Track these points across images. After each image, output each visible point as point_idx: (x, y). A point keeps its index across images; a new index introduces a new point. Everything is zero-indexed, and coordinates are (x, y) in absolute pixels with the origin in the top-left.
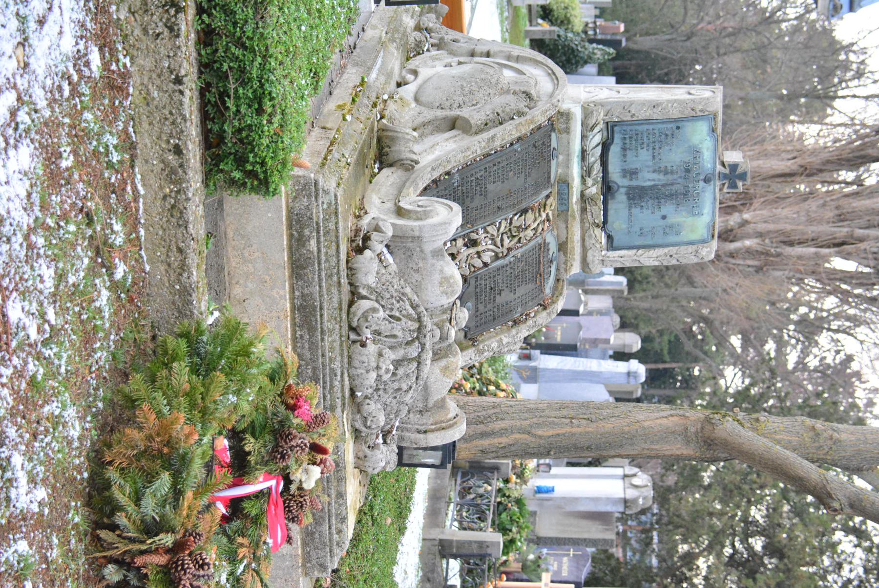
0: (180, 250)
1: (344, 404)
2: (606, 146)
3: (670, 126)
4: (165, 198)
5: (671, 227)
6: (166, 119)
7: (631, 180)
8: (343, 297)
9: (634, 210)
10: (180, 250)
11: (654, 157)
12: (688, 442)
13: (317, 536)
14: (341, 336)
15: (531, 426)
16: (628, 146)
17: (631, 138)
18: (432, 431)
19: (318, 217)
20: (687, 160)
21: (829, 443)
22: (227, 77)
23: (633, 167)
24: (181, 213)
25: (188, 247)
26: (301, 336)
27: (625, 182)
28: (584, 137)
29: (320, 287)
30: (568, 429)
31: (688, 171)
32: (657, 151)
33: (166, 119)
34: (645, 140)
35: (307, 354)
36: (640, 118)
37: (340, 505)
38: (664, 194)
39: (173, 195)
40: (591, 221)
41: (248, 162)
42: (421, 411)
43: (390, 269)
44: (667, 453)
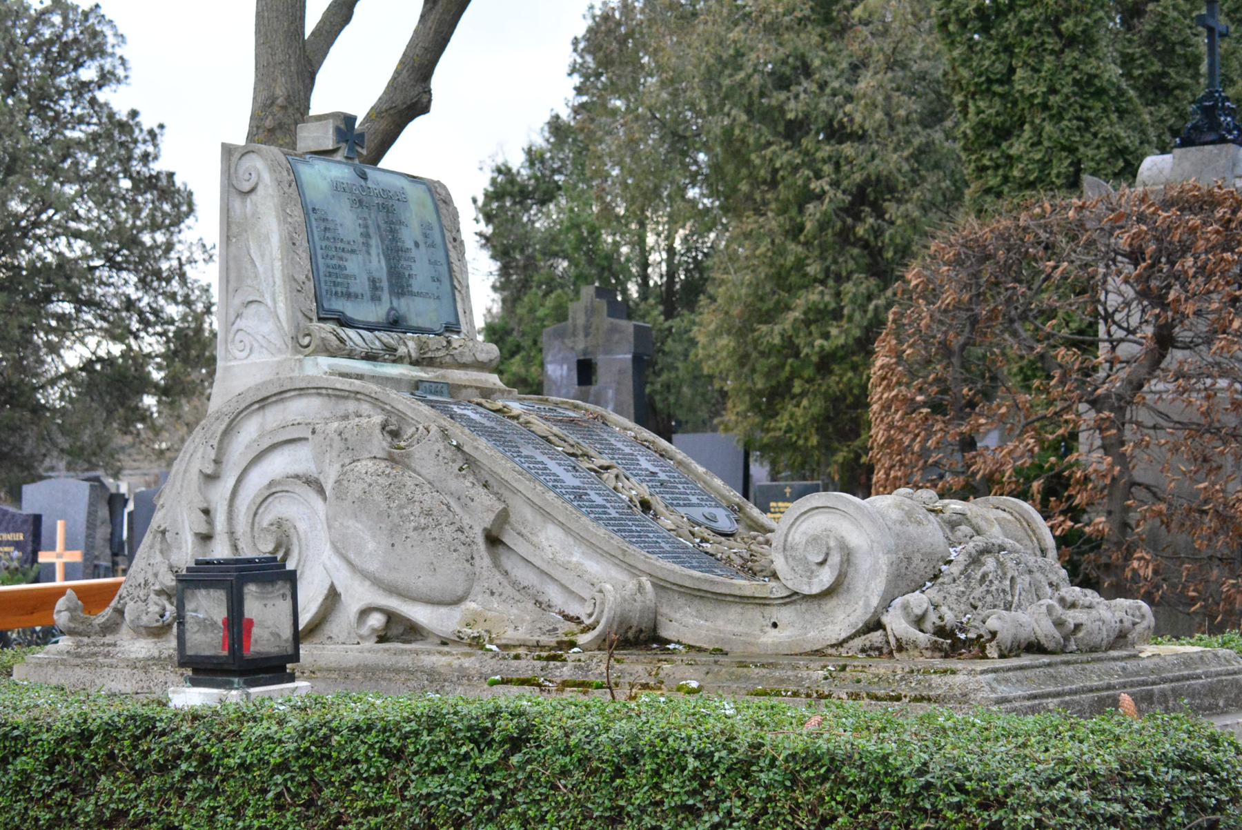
5: (426, 236)
8: (979, 668)
9: (415, 289)
17: (335, 284)
21: (290, 110)
23: (367, 283)
29: (1025, 698)
32: (348, 247)
36: (309, 267)
43: (937, 598)
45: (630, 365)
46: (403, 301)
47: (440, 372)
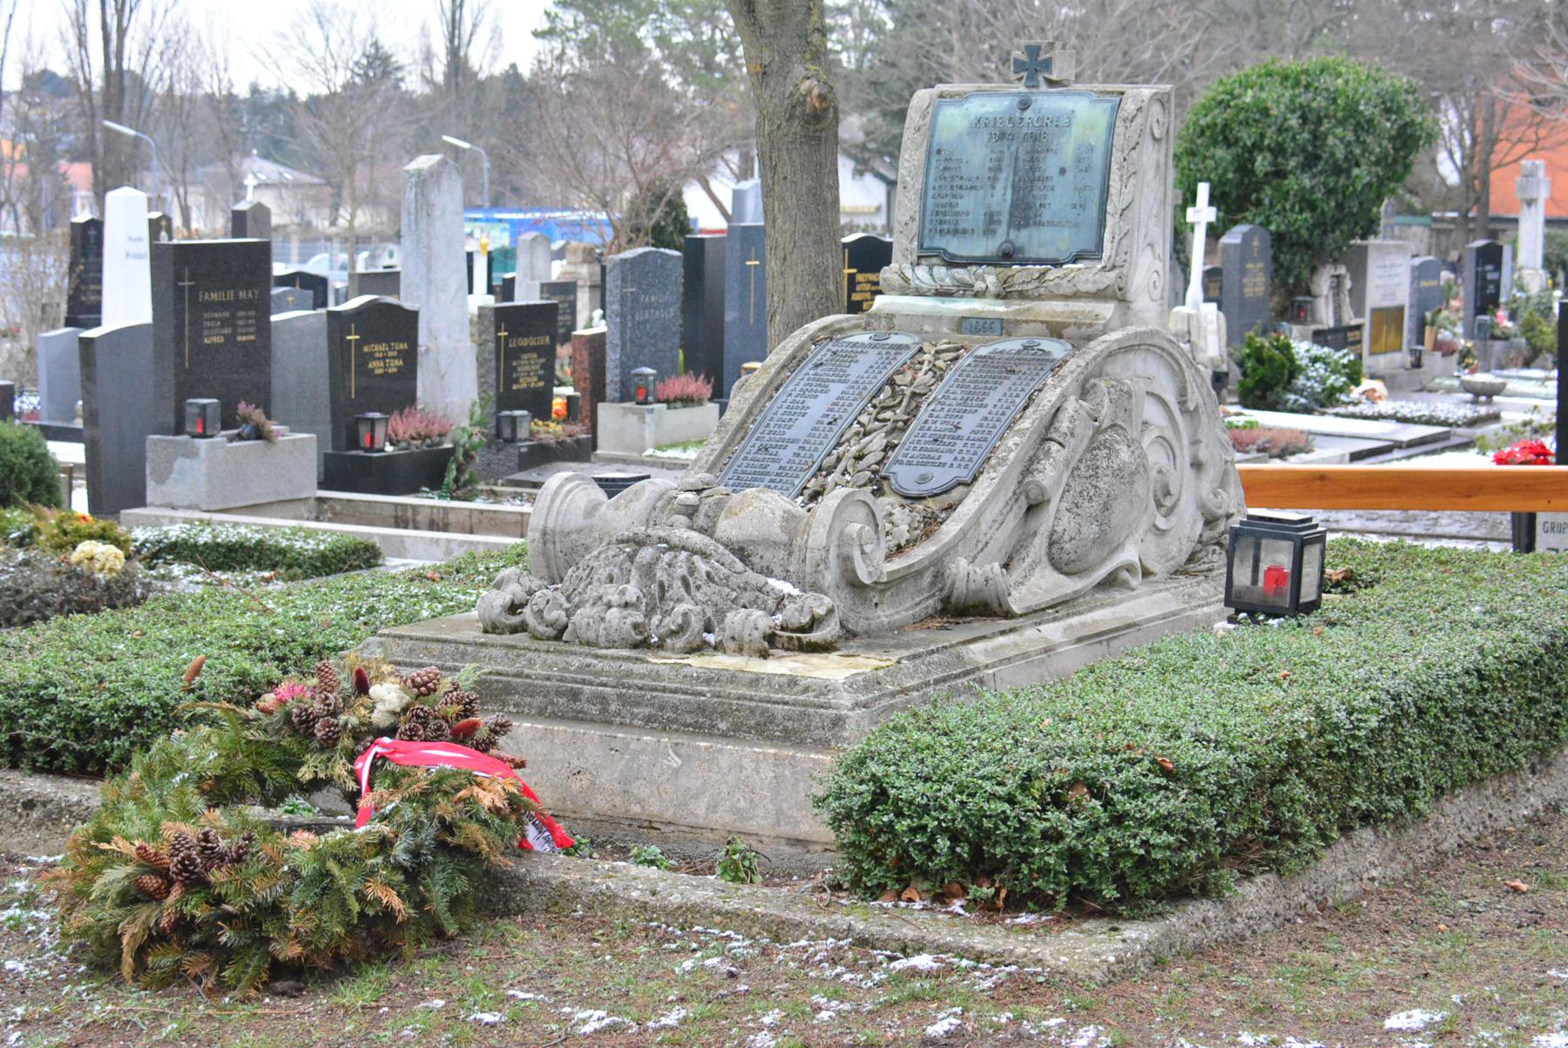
2: (952, 262)
3: (933, 161)
5: (1079, 161)
7: (999, 222)
11: (972, 188)
13: (789, 724)
16: (952, 227)
20: (986, 137)
26: (516, 705)
27: (1002, 230)
28: (919, 293)
31: (1002, 136)
34: (946, 200)
35: (538, 701)
37: (769, 683)
40: (1036, 284)
42: (790, 554)
45: (151, 485)
46: (1024, 233)
47: (1027, 304)
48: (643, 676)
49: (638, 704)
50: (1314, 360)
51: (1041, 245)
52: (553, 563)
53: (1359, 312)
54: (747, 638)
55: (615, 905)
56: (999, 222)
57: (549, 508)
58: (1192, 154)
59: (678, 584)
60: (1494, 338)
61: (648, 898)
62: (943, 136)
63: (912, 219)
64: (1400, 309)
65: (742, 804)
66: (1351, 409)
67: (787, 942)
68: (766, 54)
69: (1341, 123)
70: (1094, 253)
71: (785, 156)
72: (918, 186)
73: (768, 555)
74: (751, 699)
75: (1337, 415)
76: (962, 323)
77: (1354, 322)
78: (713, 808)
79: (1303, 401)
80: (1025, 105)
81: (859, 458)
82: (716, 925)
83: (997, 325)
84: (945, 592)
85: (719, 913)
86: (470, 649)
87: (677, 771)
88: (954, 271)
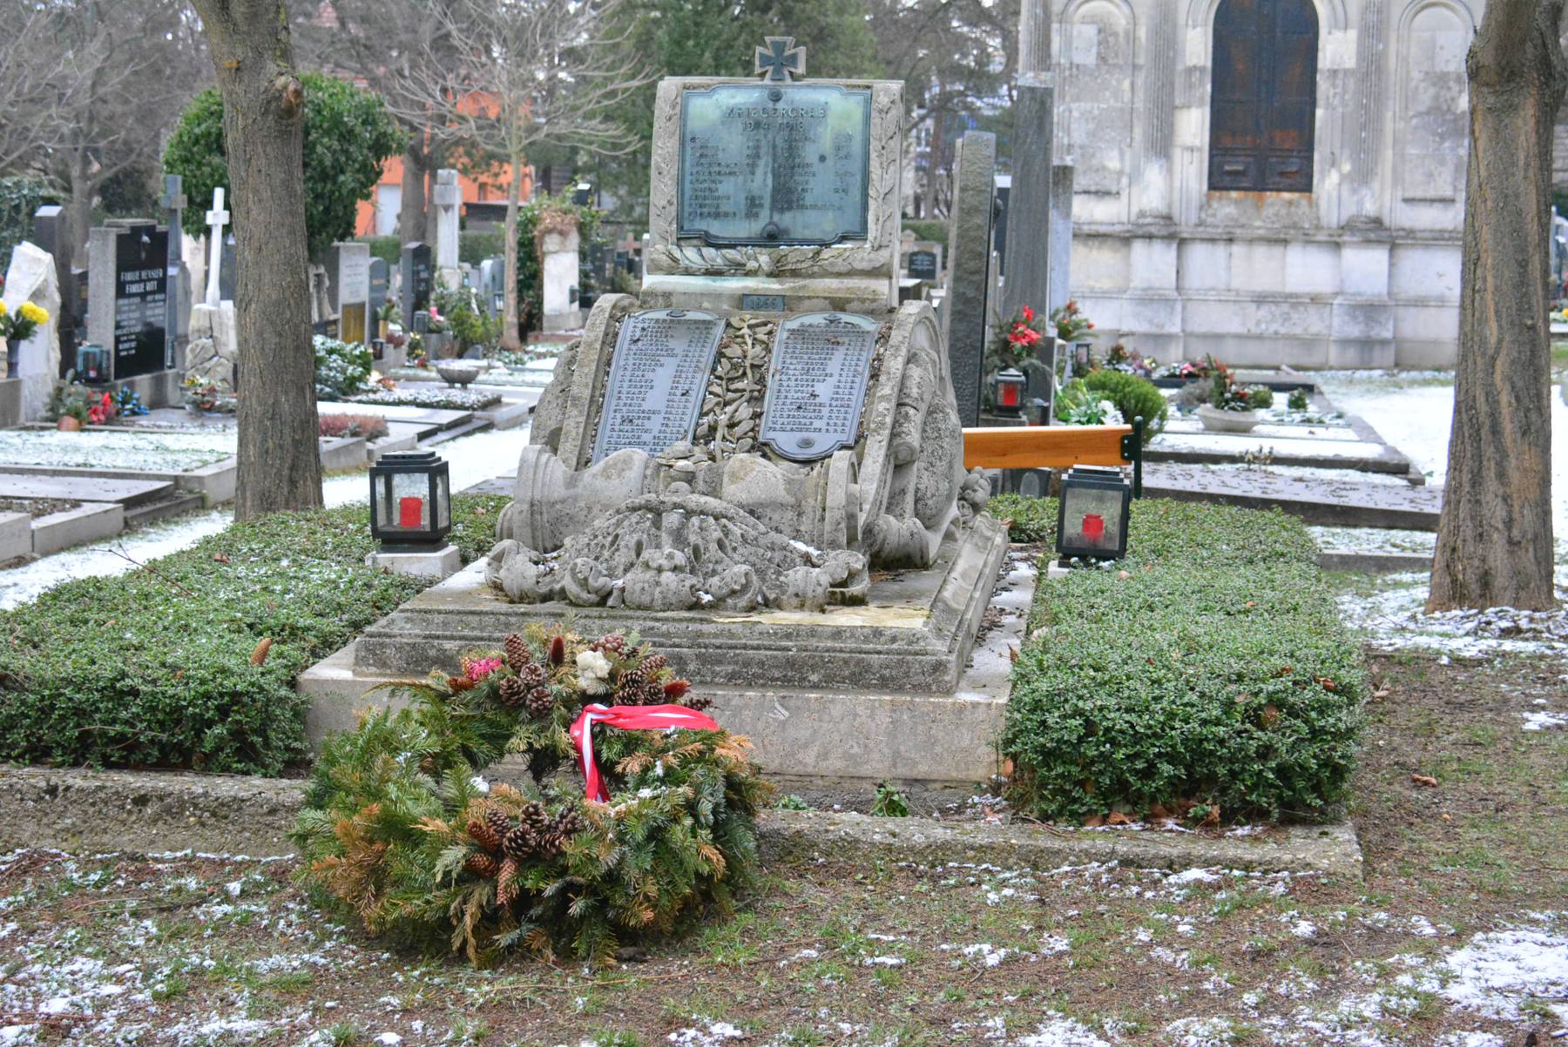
0: (273, 811)
1: (702, 620)
2: (708, 241)
3: (689, 151)
4: (203, 825)
5: (838, 148)
6: (100, 812)
7: (761, 206)
10: (273, 811)
12: (1512, 108)
13: (887, 672)
14: (600, 617)
15: (1484, 354)
18: (824, 499)
19: (417, 636)
20: (740, 127)
22: (88, 731)
24: (223, 805)
25: (268, 800)
27: (765, 214)
28: (688, 272)
30: (1489, 296)
32: (724, 170)
33: (100, 812)
37: (853, 635)
38: (787, 159)
39: (198, 813)
41: (202, 715)
42: (799, 515)
44: (1533, 140)
47: (800, 282)
48: (716, 636)
49: (720, 662)
50: (331, 352)
51: (805, 227)
52: (539, 534)
53: (335, 310)
54: (810, 594)
55: (857, 849)
56: (761, 206)
57: (534, 480)
58: (186, 161)
59: (713, 547)
60: (431, 331)
61: (891, 840)
62: (694, 125)
63: (671, 204)
64: (362, 305)
65: (856, 750)
66: (372, 396)
67: (1047, 870)
68: (239, 51)
69: (327, 133)
70: (860, 234)
71: (260, 150)
72: (674, 172)
73: (776, 517)
74: (841, 651)
75: (360, 402)
76: (743, 301)
77: (333, 317)
78: (824, 755)
79: (328, 390)
80: (776, 97)
81: (731, 426)
82: (969, 860)
83: (779, 302)
84: (876, 548)
85: (972, 848)
86: (513, 620)
87: (783, 724)
88: (724, 251)
